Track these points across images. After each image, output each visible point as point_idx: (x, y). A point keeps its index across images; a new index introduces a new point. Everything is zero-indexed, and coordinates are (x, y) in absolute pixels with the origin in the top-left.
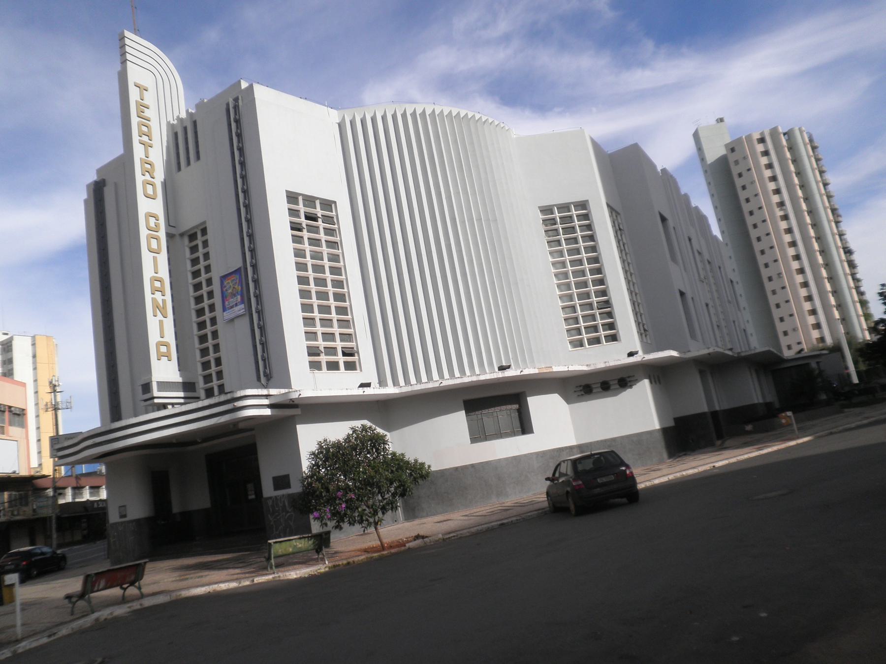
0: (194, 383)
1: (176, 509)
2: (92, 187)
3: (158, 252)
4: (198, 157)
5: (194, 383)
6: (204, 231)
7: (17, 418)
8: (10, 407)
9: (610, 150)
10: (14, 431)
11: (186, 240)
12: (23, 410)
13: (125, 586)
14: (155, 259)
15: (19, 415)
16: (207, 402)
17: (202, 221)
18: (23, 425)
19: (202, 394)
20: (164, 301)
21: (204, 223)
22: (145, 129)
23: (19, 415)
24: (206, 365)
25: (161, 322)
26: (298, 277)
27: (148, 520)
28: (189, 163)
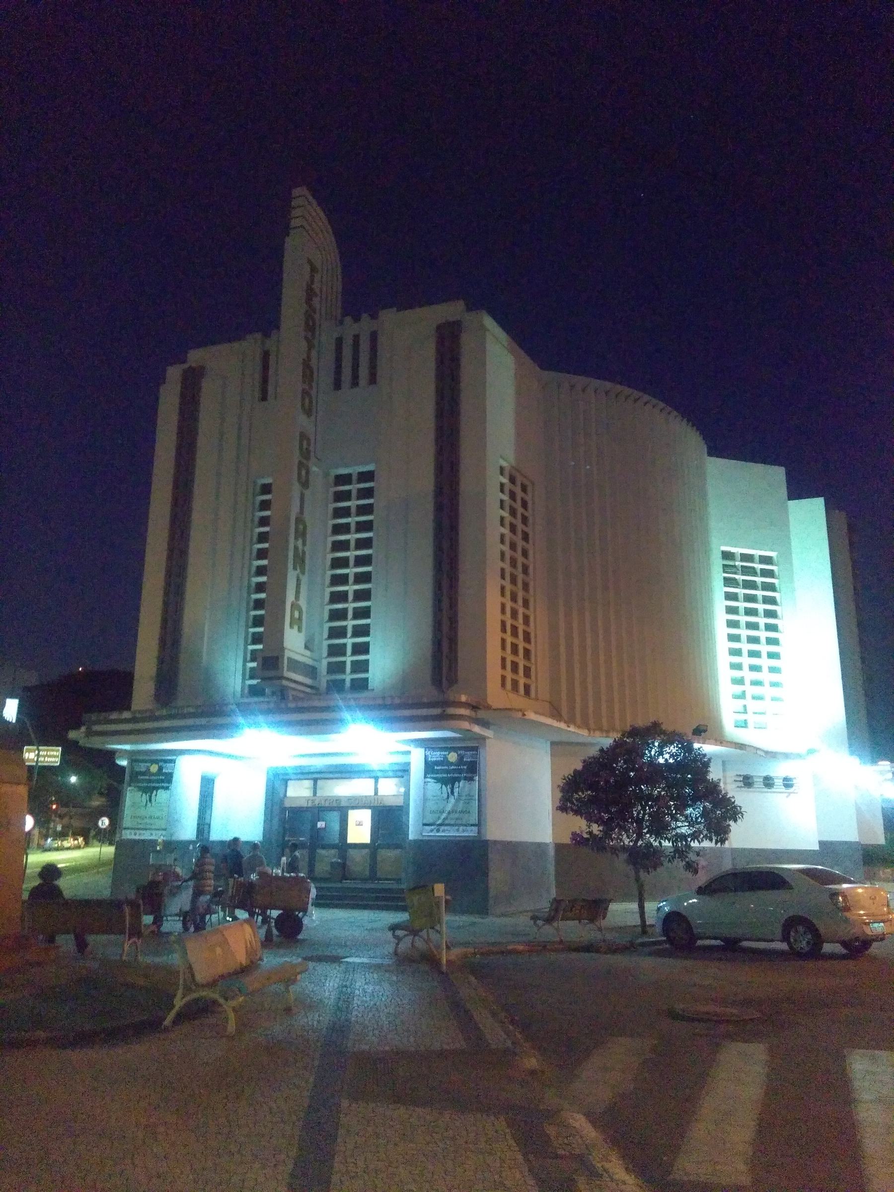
4: (373, 379)
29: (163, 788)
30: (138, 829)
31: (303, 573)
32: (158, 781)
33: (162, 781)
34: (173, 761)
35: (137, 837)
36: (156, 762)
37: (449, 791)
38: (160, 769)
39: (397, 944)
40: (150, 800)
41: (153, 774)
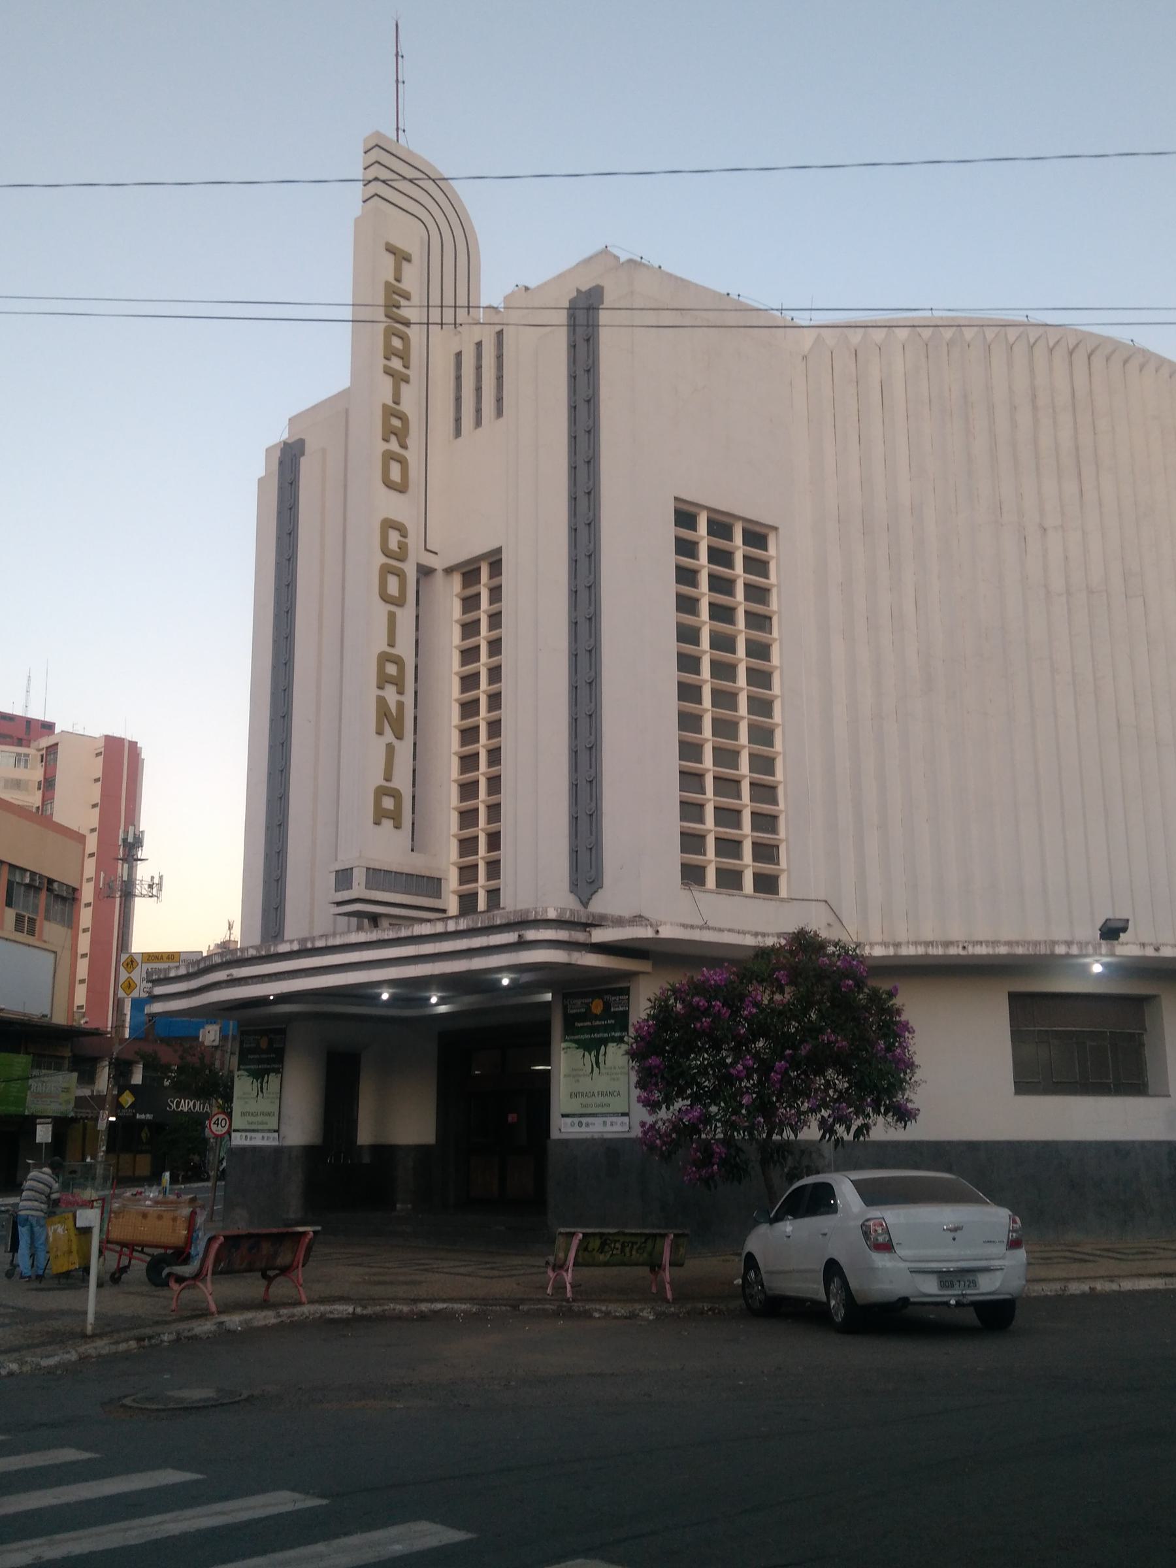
0: (439, 880)
1: (365, 1137)
2: (277, 454)
3: (399, 602)
4: (499, 413)
5: (439, 880)
6: (496, 567)
7: (59, 907)
8: (51, 881)
9: (860, 1300)
10: (52, 931)
11: (457, 580)
12: (75, 890)
13: (271, 1273)
14: (392, 617)
15: (64, 899)
16: (463, 924)
17: (494, 545)
18: (70, 922)
19: (453, 906)
20: (400, 705)
21: (499, 550)
22: (397, 343)
23: (64, 899)
24: (467, 846)
25: (390, 749)
26: (679, 683)
27: (309, 1151)
28: (478, 423)
29: (613, 1040)
30: (582, 1115)
31: (399, 736)
32: (607, 1028)
33: (612, 1028)
34: (626, 991)
35: (248, 1143)
36: (598, 994)
37: (594, 1060)
38: (607, 1006)
39: (268, 1288)
40: (598, 1066)
41: (596, 1017)
